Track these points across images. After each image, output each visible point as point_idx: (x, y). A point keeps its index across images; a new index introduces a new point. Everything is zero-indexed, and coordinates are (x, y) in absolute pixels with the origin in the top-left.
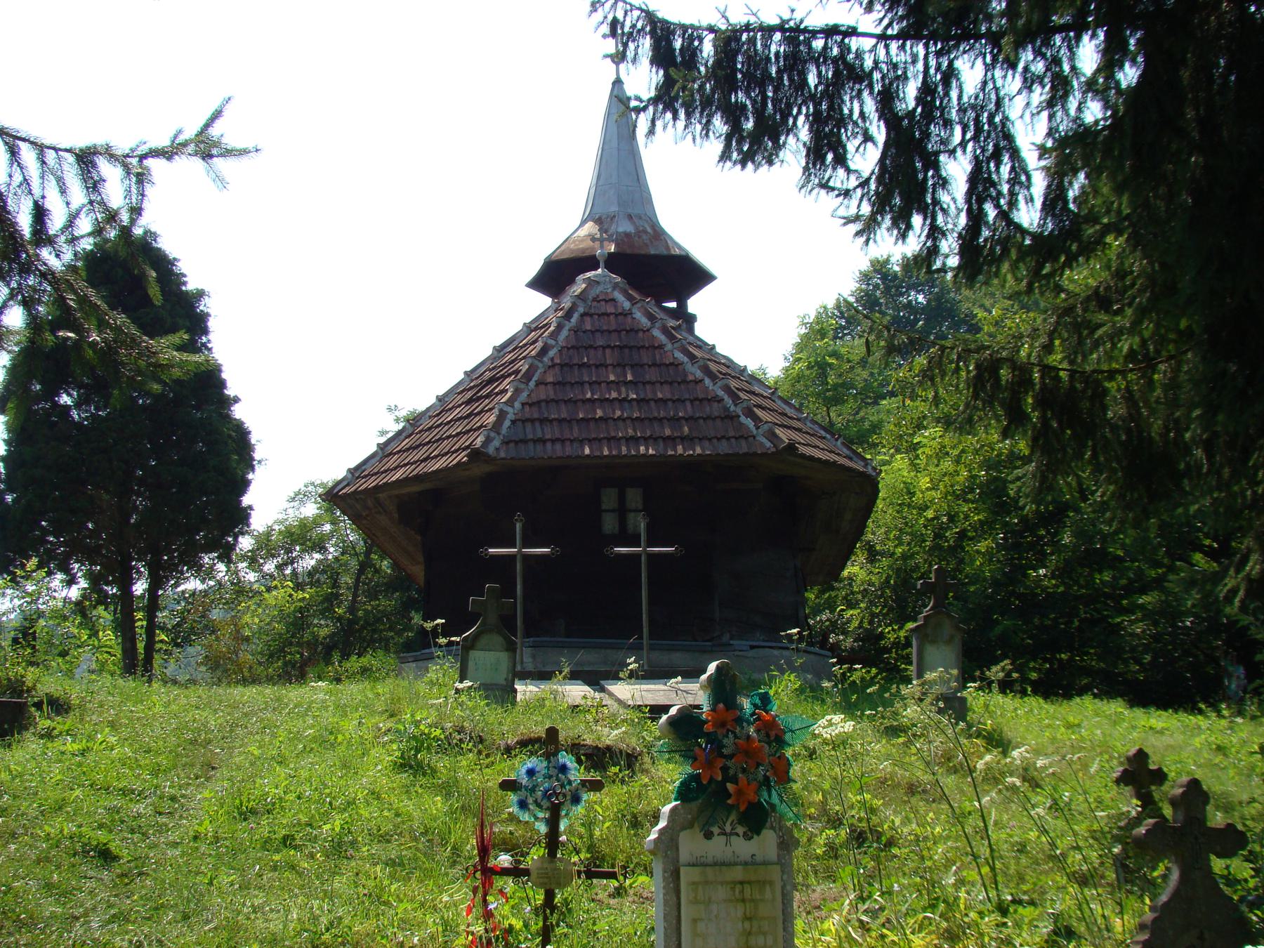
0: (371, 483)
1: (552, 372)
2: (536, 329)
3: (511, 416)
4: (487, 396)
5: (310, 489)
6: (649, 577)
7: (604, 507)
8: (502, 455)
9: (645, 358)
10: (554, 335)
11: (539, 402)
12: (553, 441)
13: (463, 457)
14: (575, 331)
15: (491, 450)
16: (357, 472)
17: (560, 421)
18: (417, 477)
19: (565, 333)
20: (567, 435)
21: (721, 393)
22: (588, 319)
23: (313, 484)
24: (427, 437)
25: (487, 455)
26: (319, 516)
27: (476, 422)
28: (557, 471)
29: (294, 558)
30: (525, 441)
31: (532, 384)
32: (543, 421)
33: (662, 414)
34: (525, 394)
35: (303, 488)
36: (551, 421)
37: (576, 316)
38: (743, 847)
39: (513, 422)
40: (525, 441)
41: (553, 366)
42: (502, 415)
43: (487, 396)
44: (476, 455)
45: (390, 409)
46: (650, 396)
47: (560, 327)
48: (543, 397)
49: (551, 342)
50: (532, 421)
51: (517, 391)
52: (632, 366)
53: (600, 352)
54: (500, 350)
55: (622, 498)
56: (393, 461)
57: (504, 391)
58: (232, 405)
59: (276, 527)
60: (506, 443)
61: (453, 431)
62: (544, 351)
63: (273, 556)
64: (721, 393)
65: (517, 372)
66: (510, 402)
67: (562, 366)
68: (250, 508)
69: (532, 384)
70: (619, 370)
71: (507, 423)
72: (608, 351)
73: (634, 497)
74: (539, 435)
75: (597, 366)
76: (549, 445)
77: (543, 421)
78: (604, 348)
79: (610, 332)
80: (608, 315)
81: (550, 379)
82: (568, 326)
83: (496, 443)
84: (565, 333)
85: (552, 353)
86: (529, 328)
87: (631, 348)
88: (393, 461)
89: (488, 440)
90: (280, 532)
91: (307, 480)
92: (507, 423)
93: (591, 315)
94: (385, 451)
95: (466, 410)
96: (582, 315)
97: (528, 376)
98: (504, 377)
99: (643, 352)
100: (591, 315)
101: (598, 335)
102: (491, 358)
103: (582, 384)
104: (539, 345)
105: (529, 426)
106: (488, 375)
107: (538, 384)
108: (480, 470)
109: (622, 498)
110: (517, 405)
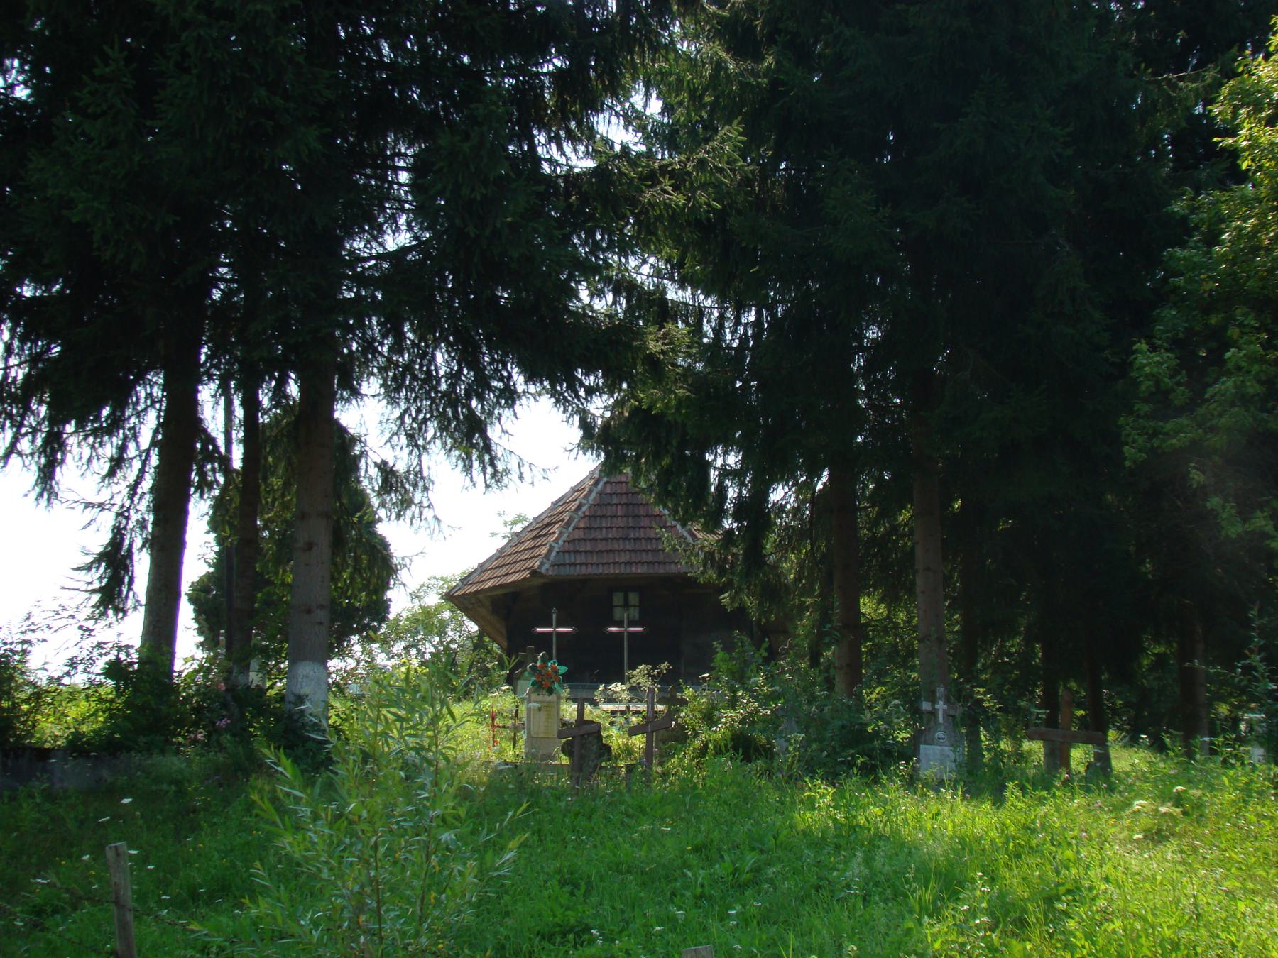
0: (474, 589)
1: (582, 521)
2: (578, 491)
3: (556, 549)
4: (544, 535)
5: (433, 581)
6: (629, 646)
7: (615, 604)
8: (550, 573)
9: (642, 511)
10: (586, 497)
11: (574, 540)
12: (581, 565)
13: (526, 574)
14: (600, 494)
15: (543, 570)
16: (466, 579)
17: (586, 552)
18: (501, 586)
19: (593, 495)
20: (590, 561)
21: (686, 534)
22: (608, 486)
23: (434, 578)
24: (508, 560)
25: (540, 573)
26: (440, 605)
27: (537, 552)
28: (585, 581)
29: (419, 641)
30: (564, 565)
31: (570, 529)
32: (575, 552)
33: (649, 547)
34: (566, 535)
35: (427, 582)
36: (580, 552)
37: (601, 484)
38: (547, 698)
39: (558, 553)
40: (564, 565)
41: (584, 517)
42: (551, 548)
43: (544, 535)
44: (534, 573)
45: (499, 514)
46: (642, 536)
47: (590, 491)
48: (577, 537)
49: (584, 501)
50: (569, 552)
51: (561, 534)
52: (633, 517)
53: (614, 508)
54: (555, 504)
55: (626, 599)
56: (487, 575)
57: (554, 533)
58: (376, 523)
59: (405, 615)
60: (553, 565)
61: (523, 557)
62: (579, 507)
63: (401, 638)
64: (686, 534)
65: (563, 520)
66: (556, 540)
67: (590, 517)
68: (208, 532)
69: (570, 529)
70: (625, 519)
71: (554, 554)
72: (619, 507)
73: (634, 598)
74: (573, 561)
75: (612, 517)
76: (578, 567)
77: (575, 552)
78: (617, 505)
79: (621, 494)
80: (622, 483)
81: (582, 525)
82: (596, 490)
83: (547, 566)
84: (593, 495)
85: (584, 509)
86: (575, 490)
87: (634, 505)
88: (487, 575)
89: (542, 564)
90: (408, 619)
91: (432, 575)
92: (554, 554)
93: (611, 483)
94: (482, 568)
95: (531, 544)
96: (605, 483)
97: (568, 524)
98: (555, 523)
99: (641, 507)
100: (611, 483)
101: (614, 496)
102: (551, 509)
103: (601, 528)
104: (577, 502)
105: (567, 555)
106: (547, 520)
107: (575, 528)
108: (537, 581)
109: (626, 599)
110: (561, 542)
